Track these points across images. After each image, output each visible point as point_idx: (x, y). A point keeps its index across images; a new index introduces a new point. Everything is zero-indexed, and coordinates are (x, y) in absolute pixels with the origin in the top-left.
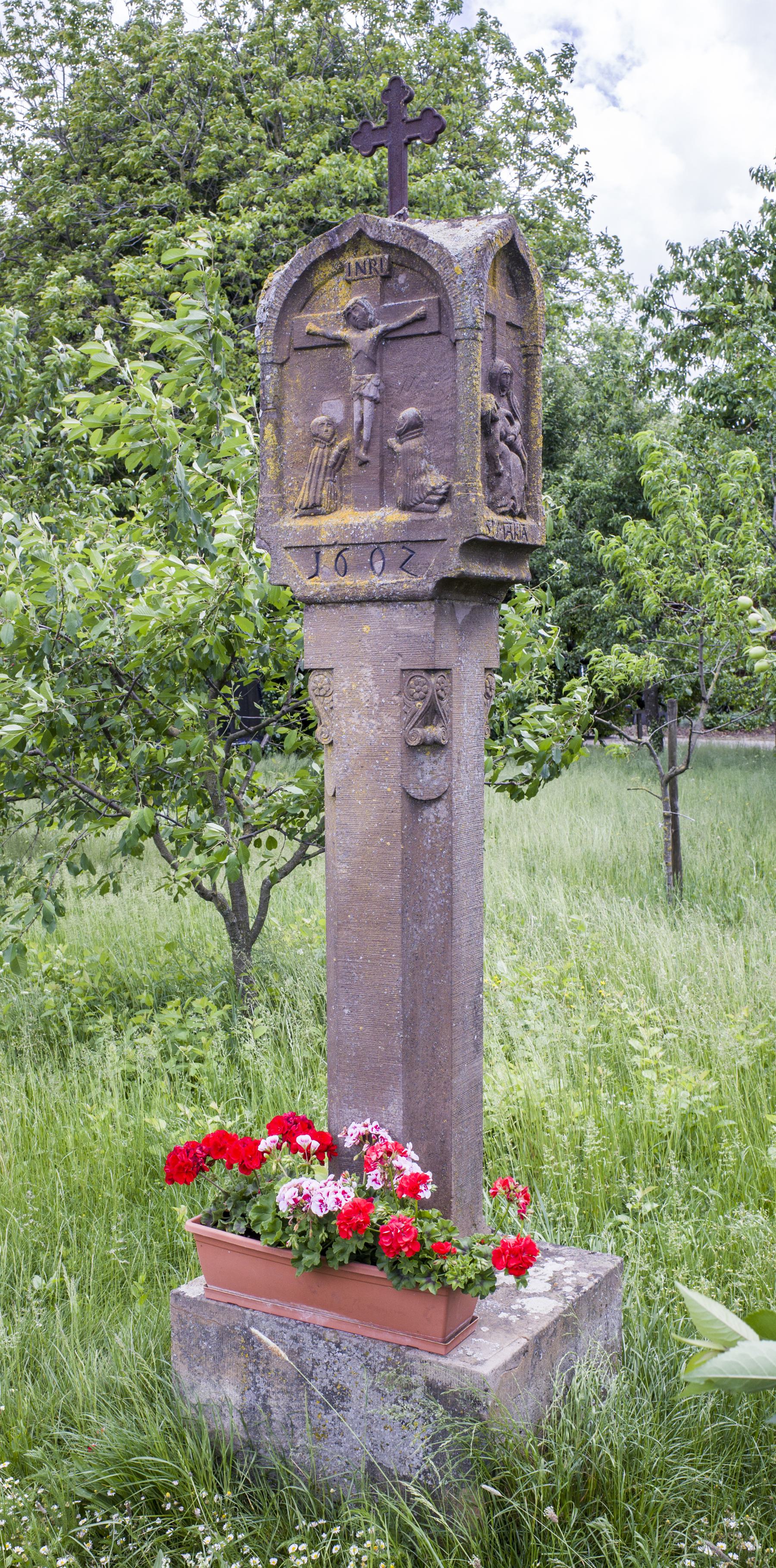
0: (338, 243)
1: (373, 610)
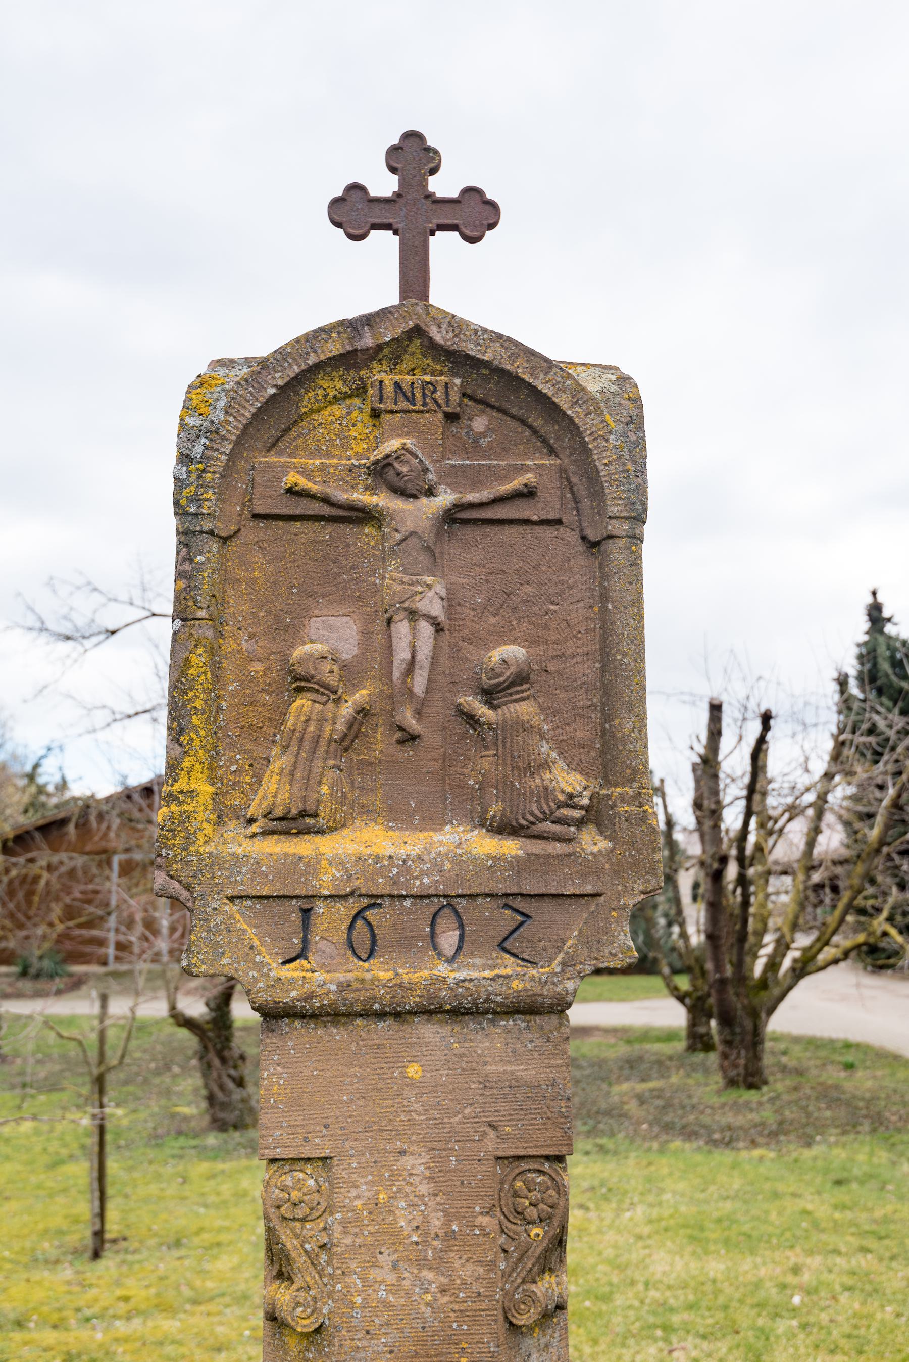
0: (368, 341)
1: (429, 1032)
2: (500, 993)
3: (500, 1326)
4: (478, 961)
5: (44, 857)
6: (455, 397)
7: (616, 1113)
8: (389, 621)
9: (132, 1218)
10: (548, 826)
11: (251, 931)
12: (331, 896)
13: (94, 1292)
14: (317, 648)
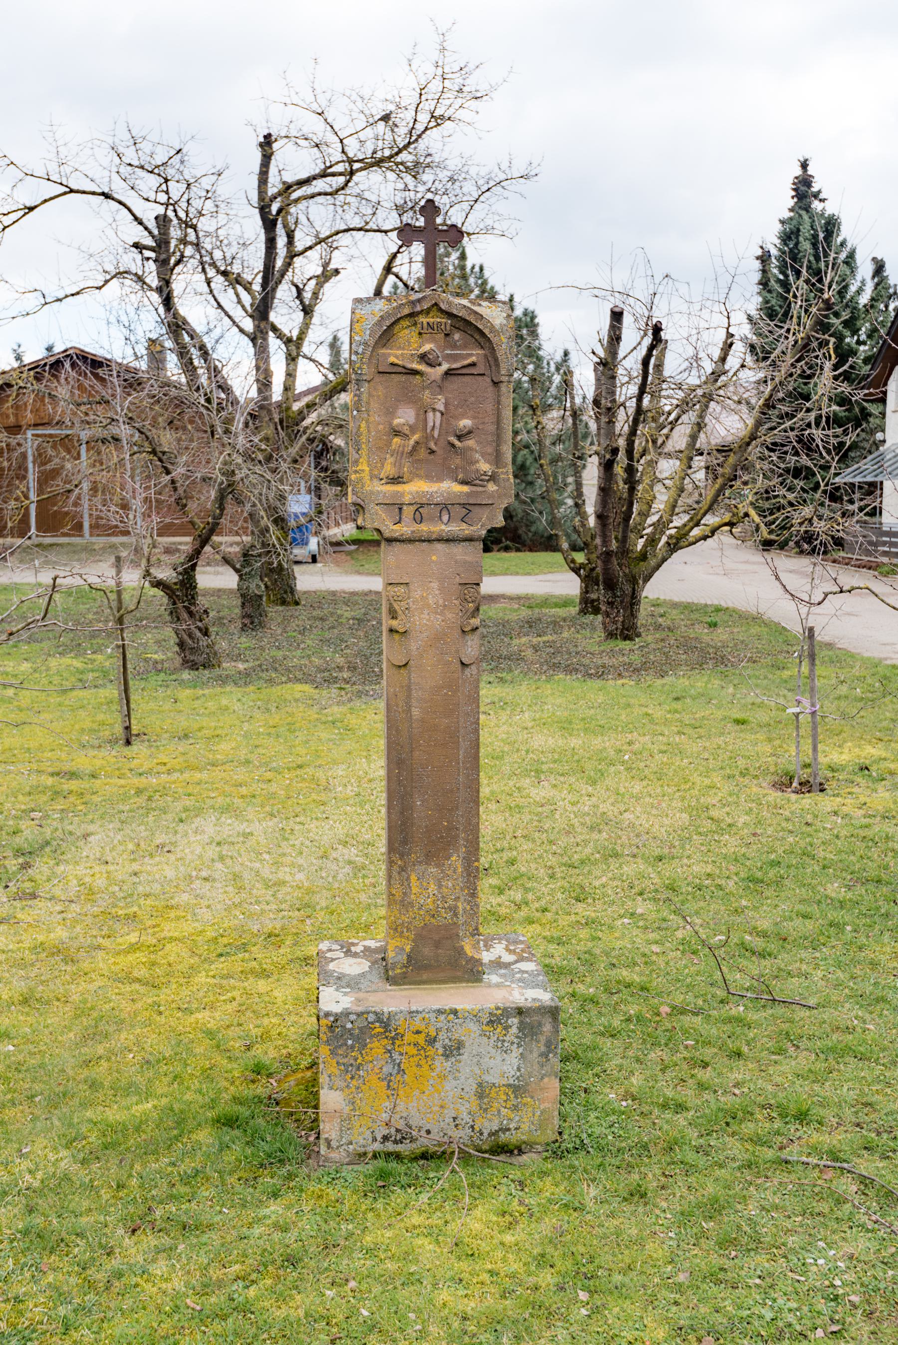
0: (418, 309)
1: (439, 546)
2: (461, 535)
6: (448, 328)
7: (517, 658)
14: (402, 421)
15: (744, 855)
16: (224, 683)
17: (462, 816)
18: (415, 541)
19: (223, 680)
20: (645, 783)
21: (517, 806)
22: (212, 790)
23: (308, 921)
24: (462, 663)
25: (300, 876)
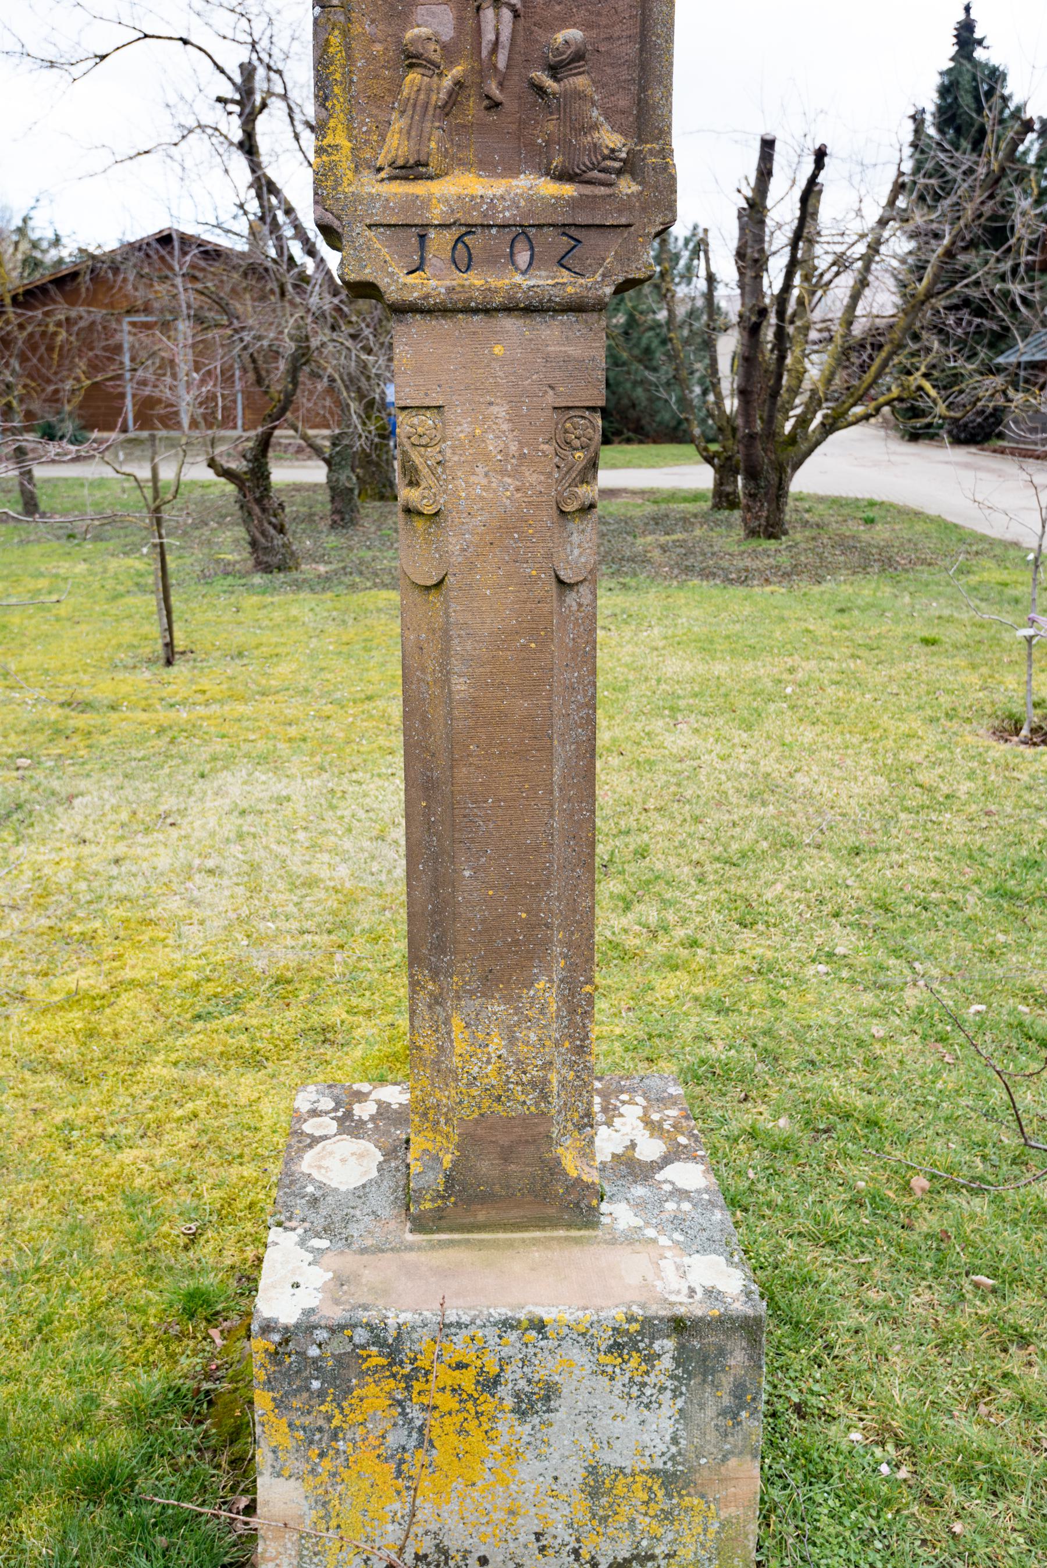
1: (509, 324)
2: (559, 296)
3: (554, 512)
4: (543, 273)
5: (61, 311)
7: (642, 560)
8: (478, 8)
9: (196, 636)
10: (595, 174)
11: (384, 251)
12: (440, 225)
13: (171, 688)
14: (424, 31)
15: (980, 849)
16: (299, 588)
17: (558, 898)
18: (455, 311)
19: (298, 586)
20: (819, 728)
21: (647, 761)
22: (253, 731)
23: (338, 957)
24: (560, 582)
25: (343, 871)
